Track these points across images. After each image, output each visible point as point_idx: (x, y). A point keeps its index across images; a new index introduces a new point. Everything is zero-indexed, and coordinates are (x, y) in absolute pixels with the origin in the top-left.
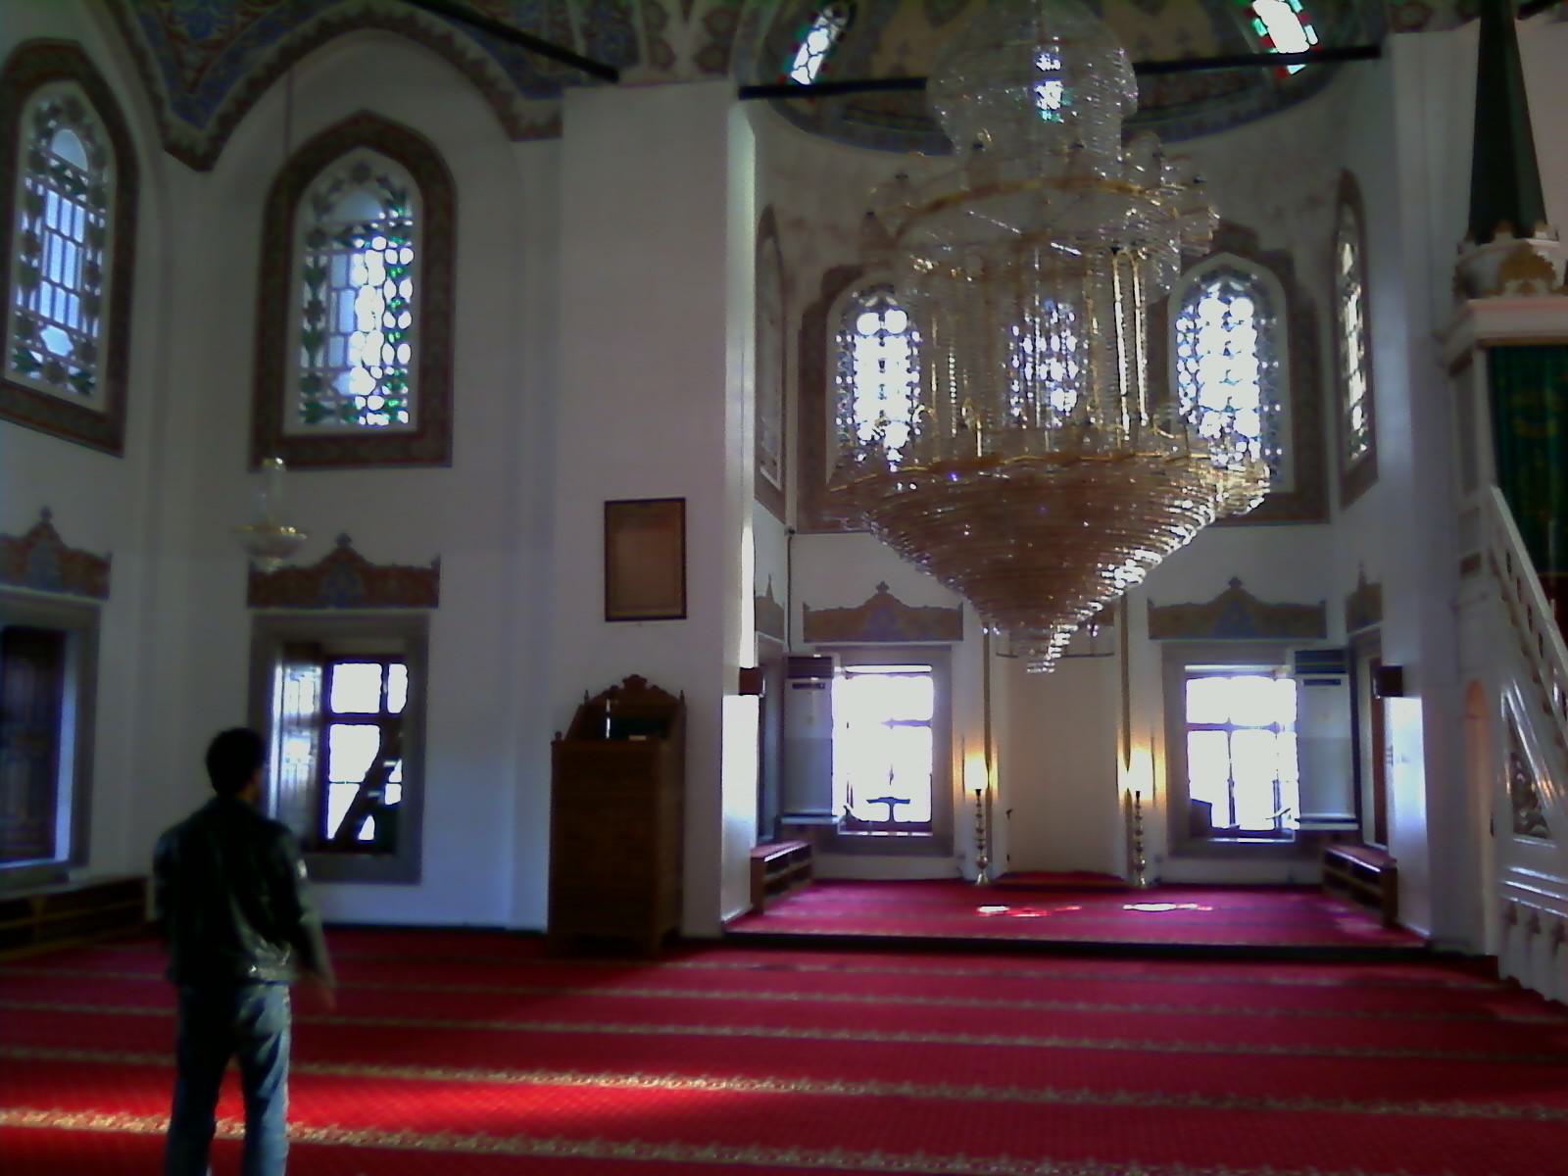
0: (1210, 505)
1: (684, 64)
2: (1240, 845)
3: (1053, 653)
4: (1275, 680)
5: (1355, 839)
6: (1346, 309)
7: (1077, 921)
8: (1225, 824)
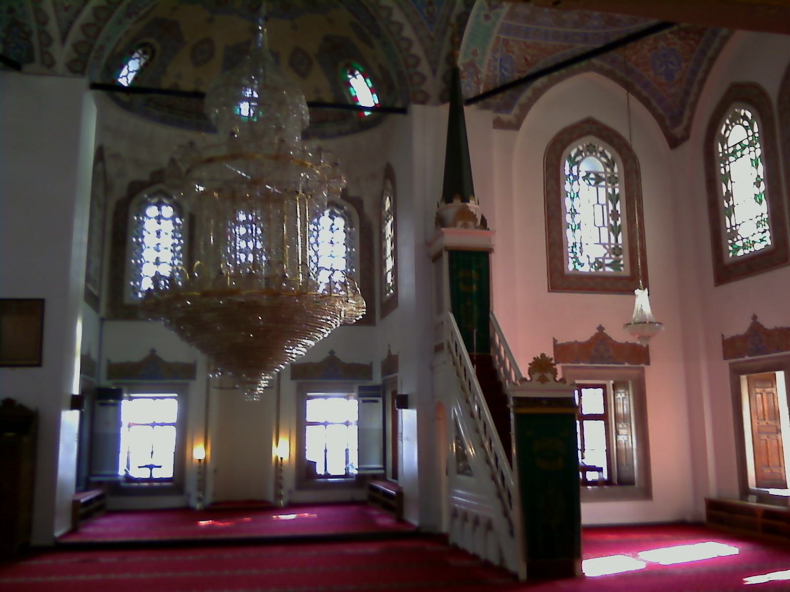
0: (338, 319)
1: (60, 66)
2: (326, 483)
3: (259, 390)
4: (348, 400)
5: (382, 478)
6: (386, 227)
7: (249, 526)
8: (323, 473)
